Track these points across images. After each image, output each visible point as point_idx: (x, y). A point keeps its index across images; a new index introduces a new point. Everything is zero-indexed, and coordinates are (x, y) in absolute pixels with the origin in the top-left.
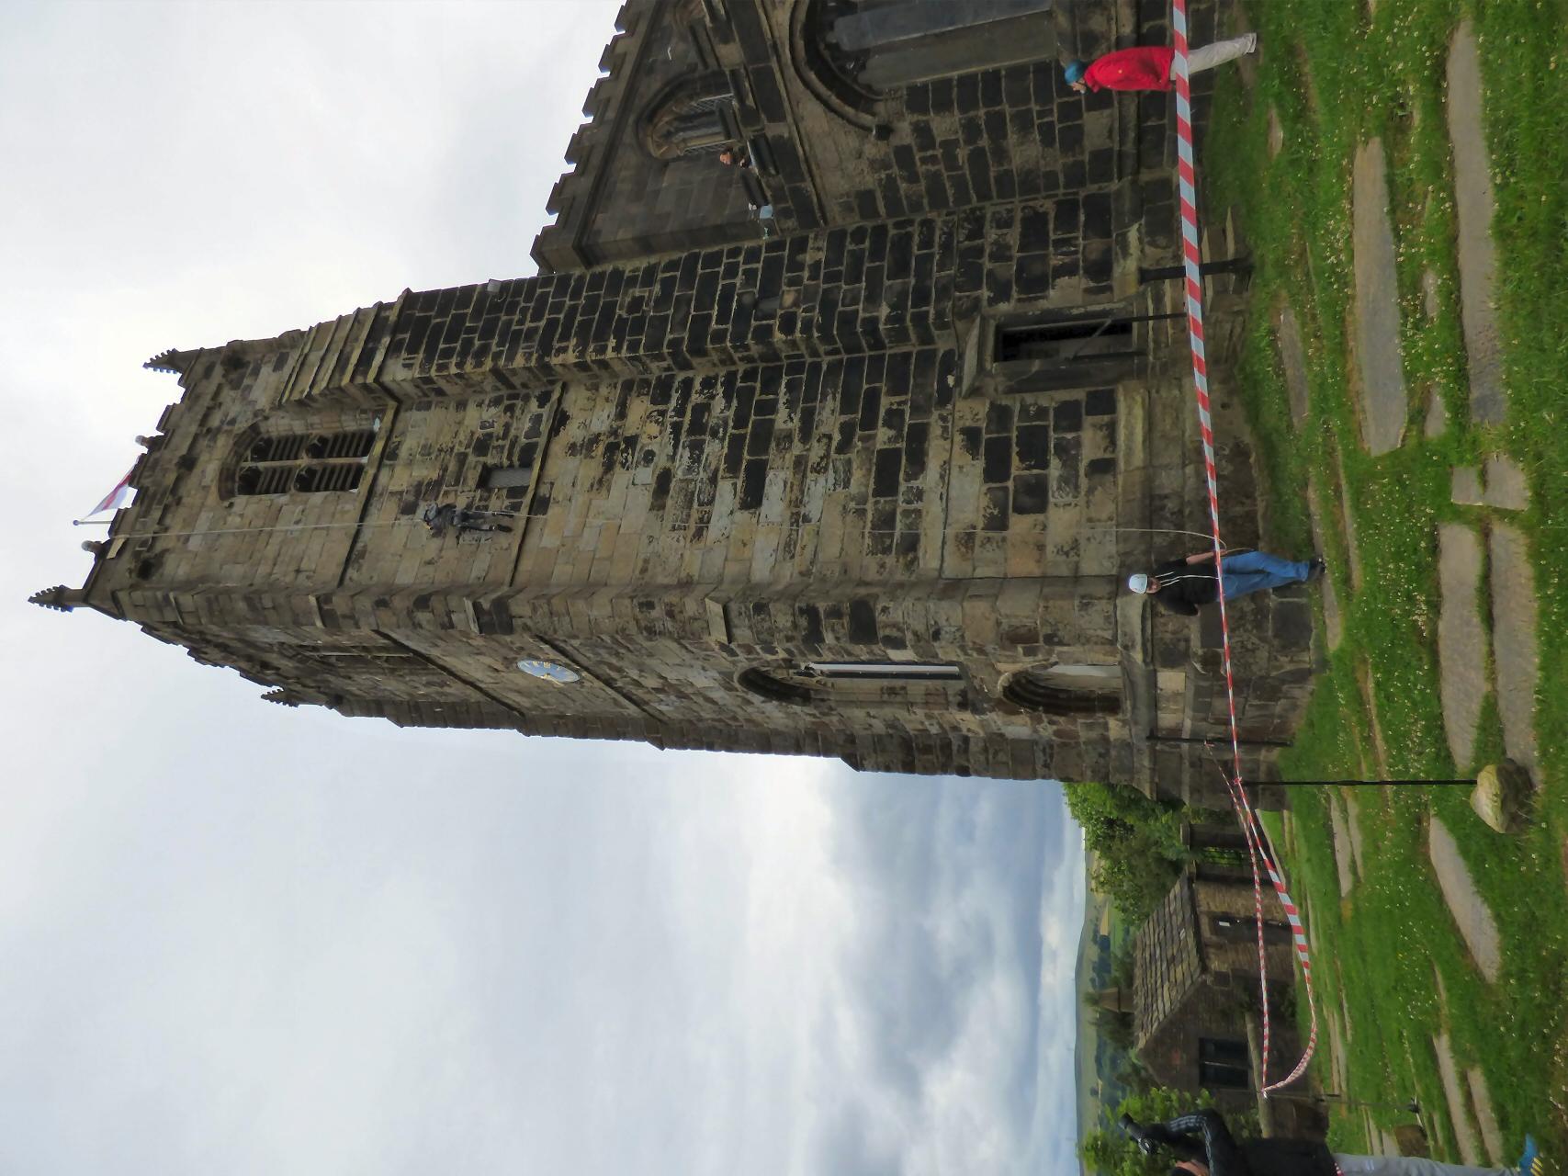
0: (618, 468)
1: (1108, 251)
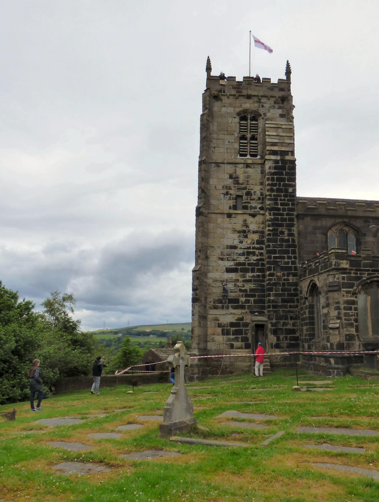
0: (239, 234)
1: (283, 348)
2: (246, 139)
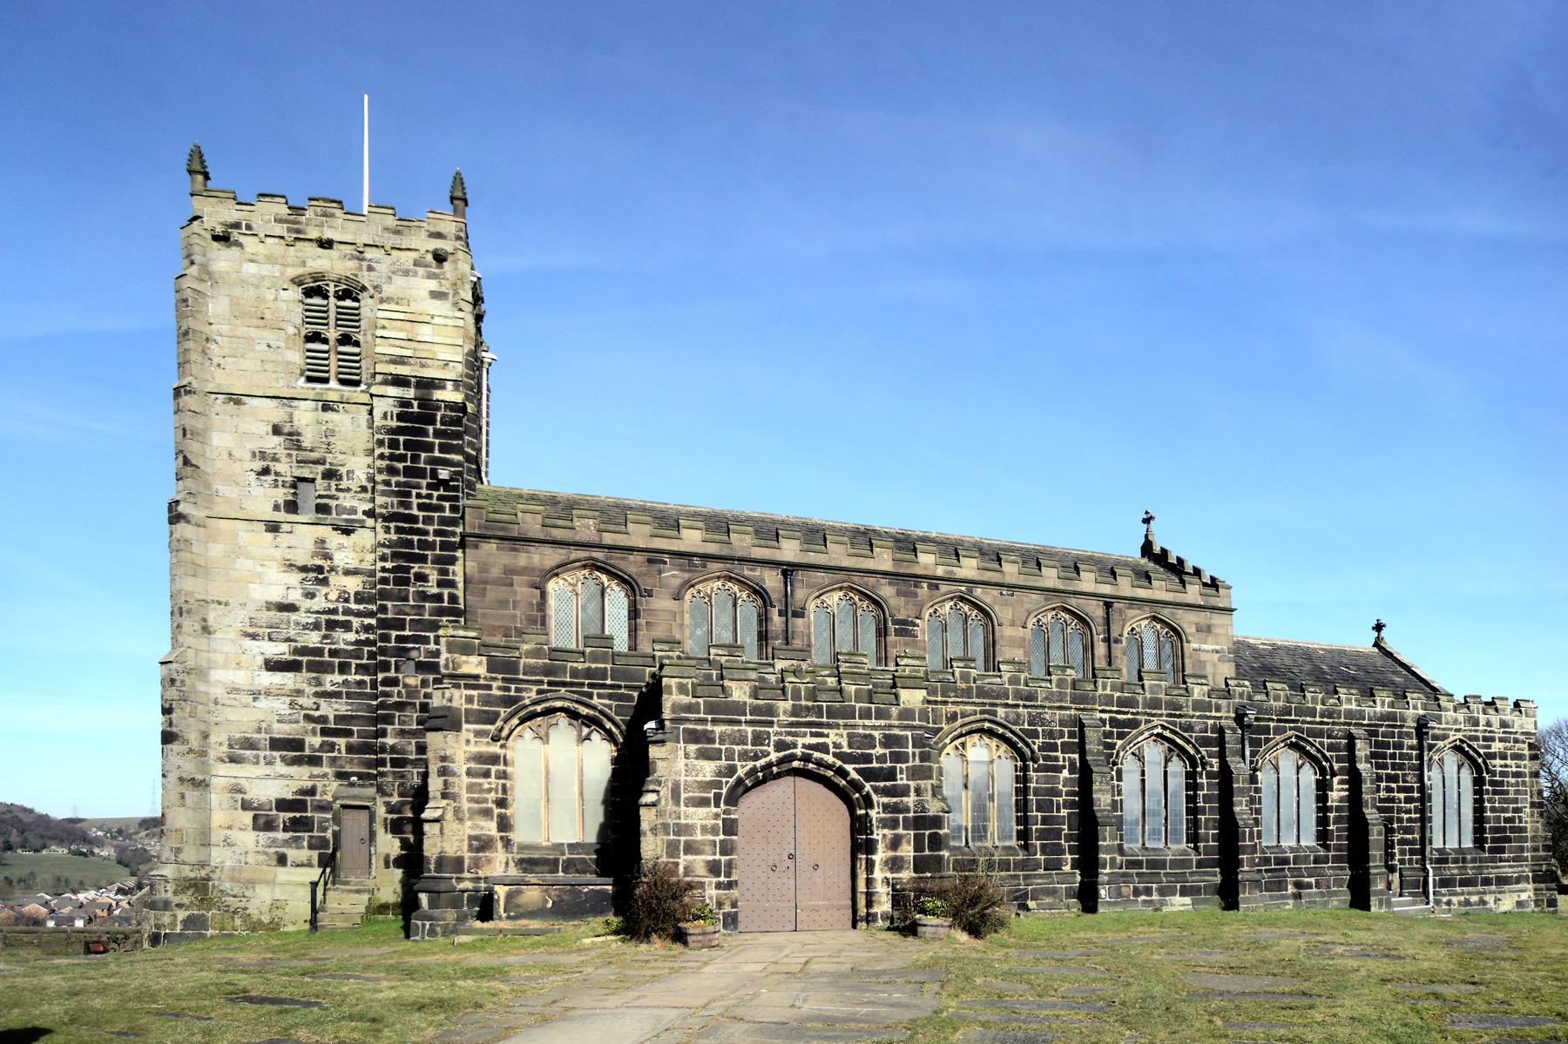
0: (304, 575)
2: (325, 341)
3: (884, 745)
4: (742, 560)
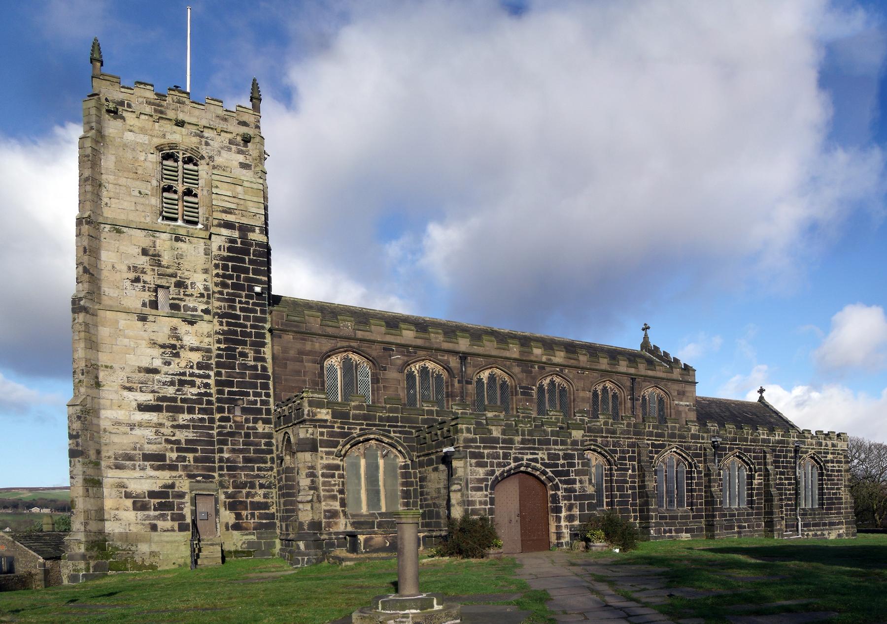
0: (163, 350)
2: (175, 192)
3: (564, 459)
4: (437, 350)
